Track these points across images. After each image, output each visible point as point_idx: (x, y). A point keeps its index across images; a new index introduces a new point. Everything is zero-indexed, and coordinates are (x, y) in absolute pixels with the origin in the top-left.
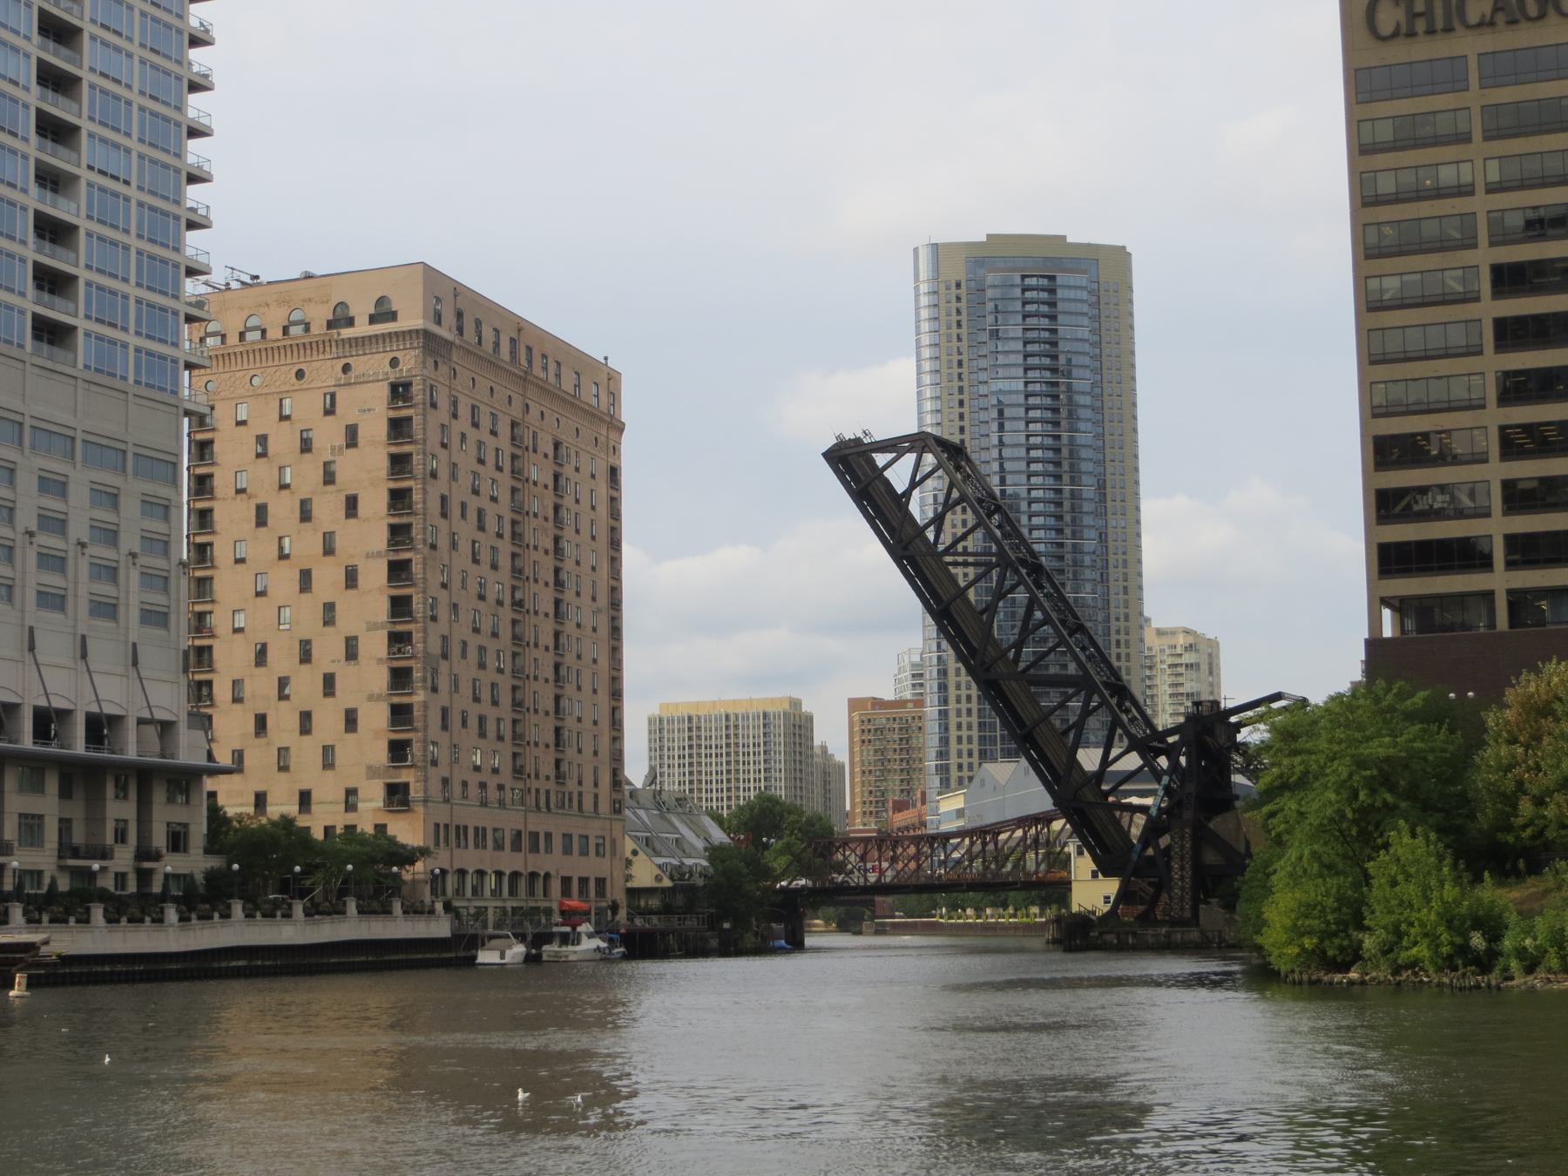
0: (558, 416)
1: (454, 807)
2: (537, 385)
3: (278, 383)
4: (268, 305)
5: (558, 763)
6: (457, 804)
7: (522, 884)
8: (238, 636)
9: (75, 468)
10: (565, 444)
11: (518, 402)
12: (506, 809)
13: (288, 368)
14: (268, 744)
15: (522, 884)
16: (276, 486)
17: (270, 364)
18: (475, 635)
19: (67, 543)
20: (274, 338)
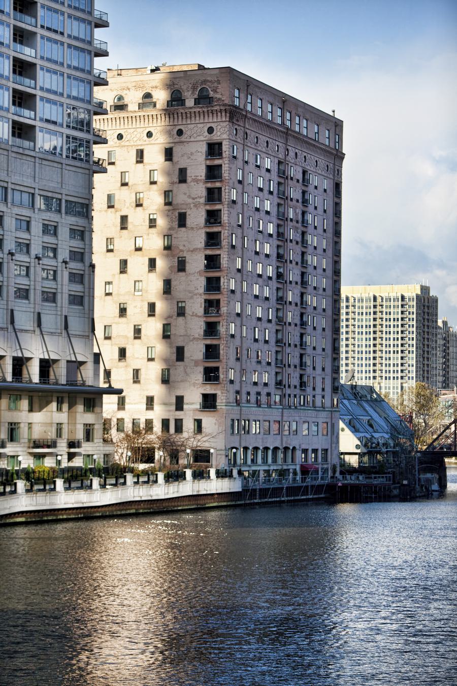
0: (305, 154)
1: (242, 408)
2: (294, 137)
3: (135, 139)
4: (129, 89)
5: (301, 376)
6: (243, 406)
7: (280, 455)
8: (109, 297)
9: (34, 212)
10: (309, 172)
11: (282, 150)
12: (271, 408)
13: (142, 129)
14: (126, 366)
15: (280, 455)
16: (134, 205)
17: (130, 127)
18: (256, 300)
19: (30, 257)
20: (132, 110)
